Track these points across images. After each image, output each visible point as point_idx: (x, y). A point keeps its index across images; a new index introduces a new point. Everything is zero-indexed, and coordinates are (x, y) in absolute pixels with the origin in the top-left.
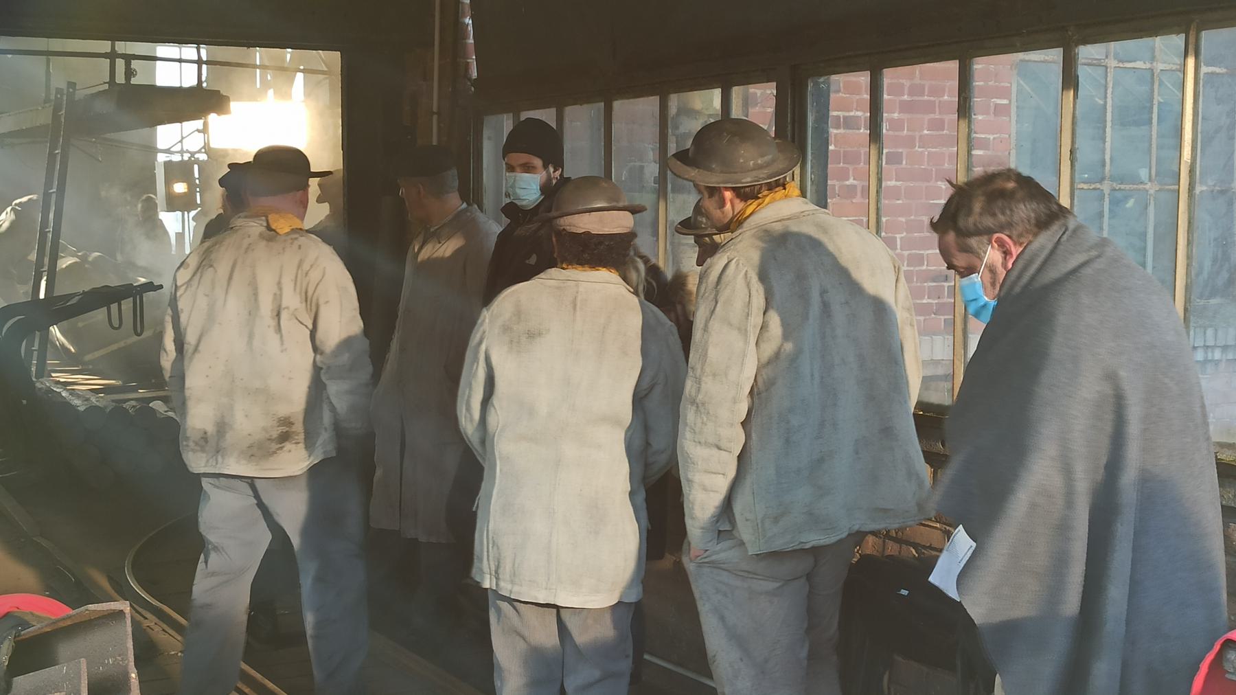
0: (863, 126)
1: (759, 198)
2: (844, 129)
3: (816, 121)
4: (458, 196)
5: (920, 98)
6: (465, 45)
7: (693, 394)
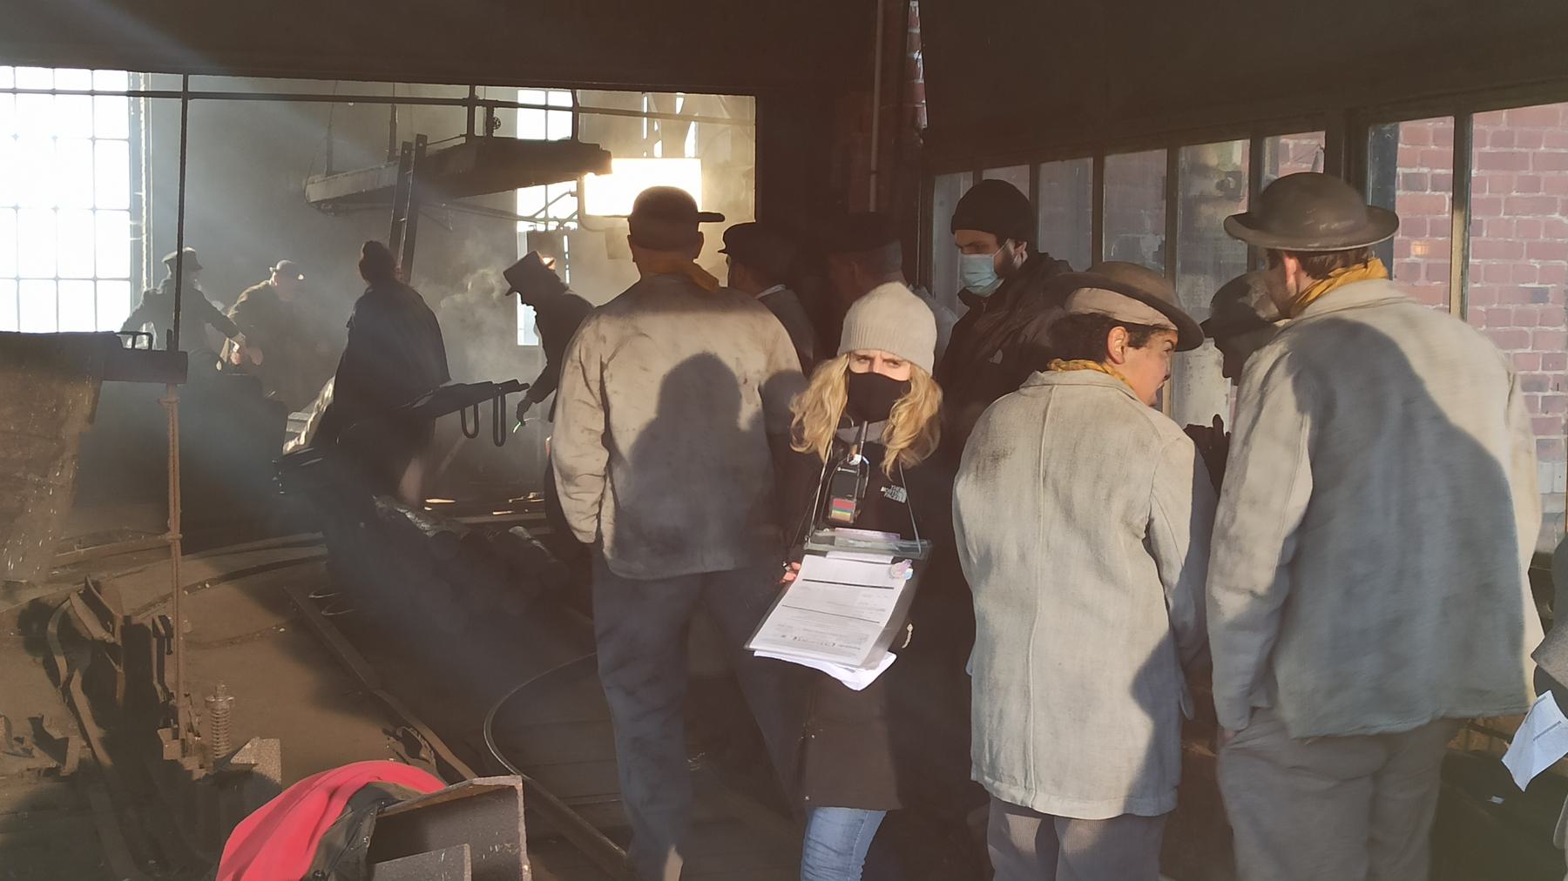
0: (1429, 186)
1: (1330, 277)
2: (1404, 190)
4: (902, 275)
7: (1226, 524)
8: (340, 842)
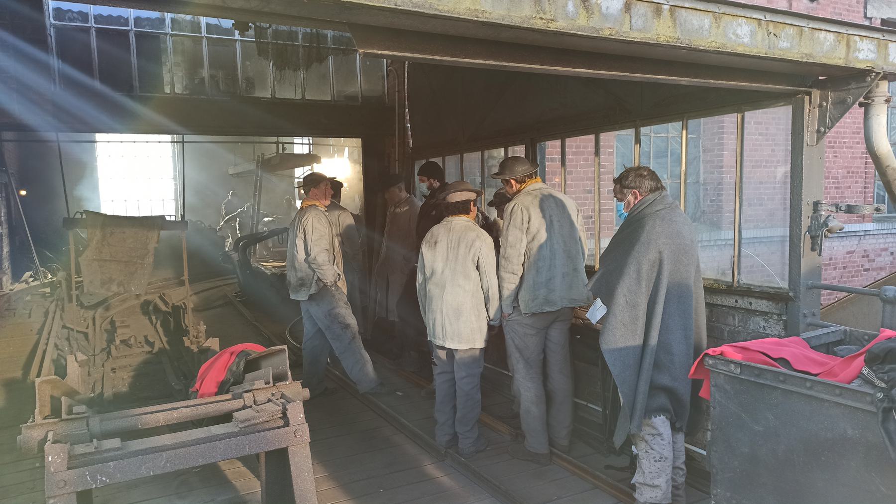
3: (540, 159)
5: (579, 150)
6: (408, 135)
8: (234, 369)
